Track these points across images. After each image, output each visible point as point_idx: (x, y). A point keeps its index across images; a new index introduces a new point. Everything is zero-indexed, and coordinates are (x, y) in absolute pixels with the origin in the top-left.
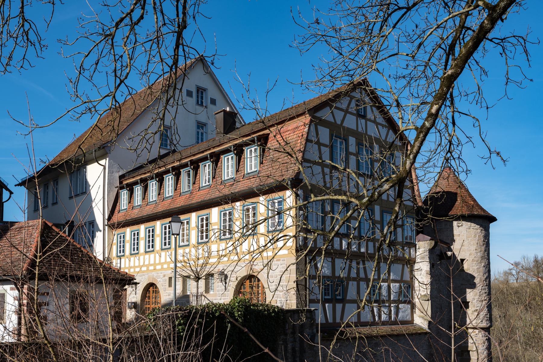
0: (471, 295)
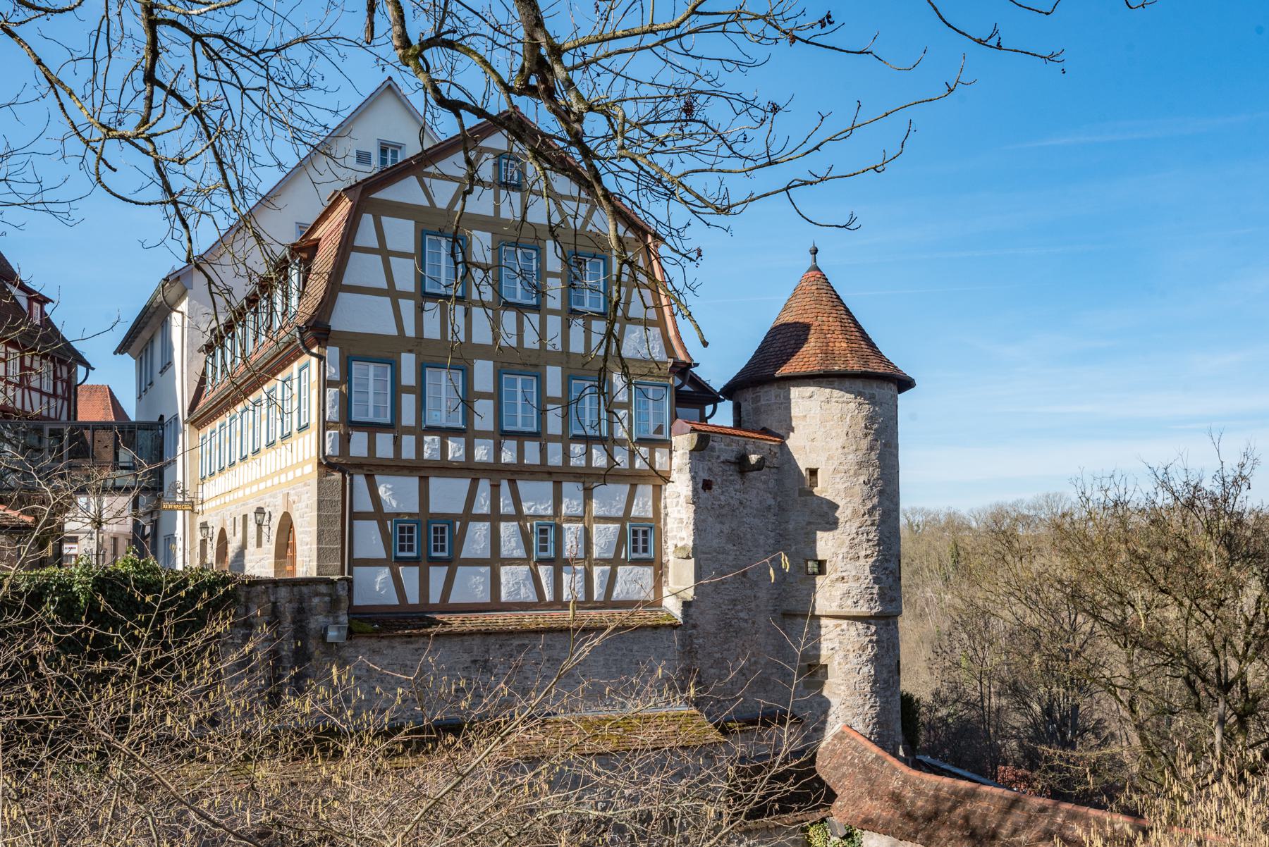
0: (827, 545)
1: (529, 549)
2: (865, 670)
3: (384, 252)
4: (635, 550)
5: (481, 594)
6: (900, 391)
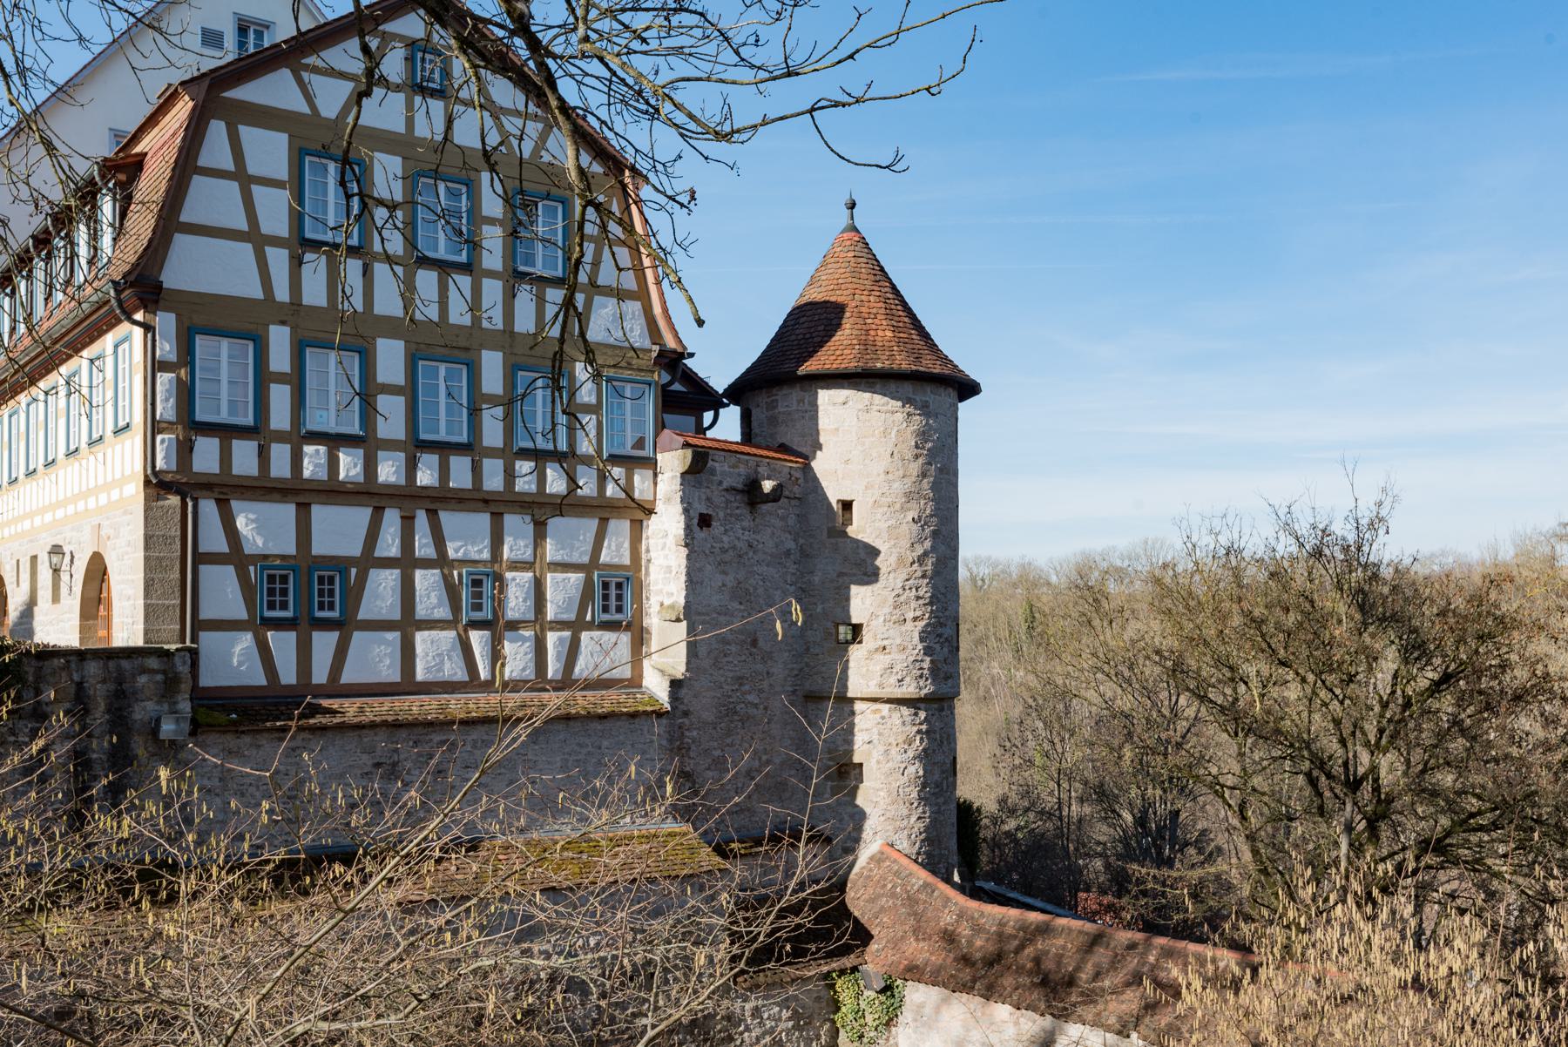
0: (863, 603)
1: (455, 606)
3: (243, 178)
4: (605, 609)
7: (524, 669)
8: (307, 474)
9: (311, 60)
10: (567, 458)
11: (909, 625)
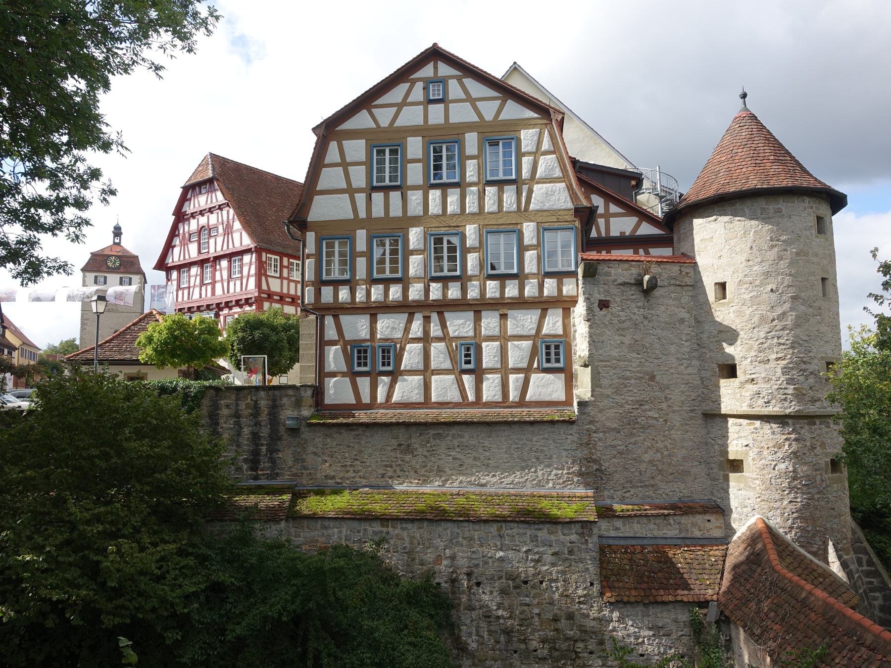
1: (453, 360)
2: (782, 466)
3: (344, 164)
4: (548, 361)
5: (417, 396)
6: (835, 211)
7: (494, 396)
8: (526, 294)
9: (380, 101)
10: (520, 277)
11: (772, 364)
